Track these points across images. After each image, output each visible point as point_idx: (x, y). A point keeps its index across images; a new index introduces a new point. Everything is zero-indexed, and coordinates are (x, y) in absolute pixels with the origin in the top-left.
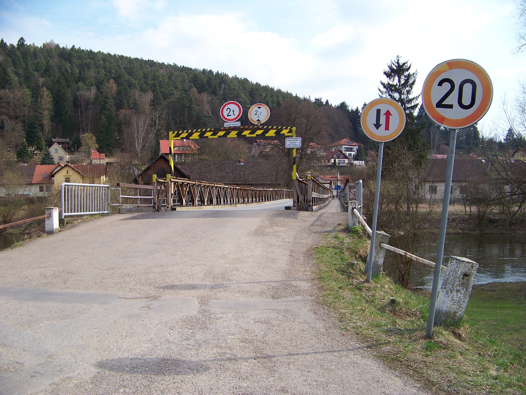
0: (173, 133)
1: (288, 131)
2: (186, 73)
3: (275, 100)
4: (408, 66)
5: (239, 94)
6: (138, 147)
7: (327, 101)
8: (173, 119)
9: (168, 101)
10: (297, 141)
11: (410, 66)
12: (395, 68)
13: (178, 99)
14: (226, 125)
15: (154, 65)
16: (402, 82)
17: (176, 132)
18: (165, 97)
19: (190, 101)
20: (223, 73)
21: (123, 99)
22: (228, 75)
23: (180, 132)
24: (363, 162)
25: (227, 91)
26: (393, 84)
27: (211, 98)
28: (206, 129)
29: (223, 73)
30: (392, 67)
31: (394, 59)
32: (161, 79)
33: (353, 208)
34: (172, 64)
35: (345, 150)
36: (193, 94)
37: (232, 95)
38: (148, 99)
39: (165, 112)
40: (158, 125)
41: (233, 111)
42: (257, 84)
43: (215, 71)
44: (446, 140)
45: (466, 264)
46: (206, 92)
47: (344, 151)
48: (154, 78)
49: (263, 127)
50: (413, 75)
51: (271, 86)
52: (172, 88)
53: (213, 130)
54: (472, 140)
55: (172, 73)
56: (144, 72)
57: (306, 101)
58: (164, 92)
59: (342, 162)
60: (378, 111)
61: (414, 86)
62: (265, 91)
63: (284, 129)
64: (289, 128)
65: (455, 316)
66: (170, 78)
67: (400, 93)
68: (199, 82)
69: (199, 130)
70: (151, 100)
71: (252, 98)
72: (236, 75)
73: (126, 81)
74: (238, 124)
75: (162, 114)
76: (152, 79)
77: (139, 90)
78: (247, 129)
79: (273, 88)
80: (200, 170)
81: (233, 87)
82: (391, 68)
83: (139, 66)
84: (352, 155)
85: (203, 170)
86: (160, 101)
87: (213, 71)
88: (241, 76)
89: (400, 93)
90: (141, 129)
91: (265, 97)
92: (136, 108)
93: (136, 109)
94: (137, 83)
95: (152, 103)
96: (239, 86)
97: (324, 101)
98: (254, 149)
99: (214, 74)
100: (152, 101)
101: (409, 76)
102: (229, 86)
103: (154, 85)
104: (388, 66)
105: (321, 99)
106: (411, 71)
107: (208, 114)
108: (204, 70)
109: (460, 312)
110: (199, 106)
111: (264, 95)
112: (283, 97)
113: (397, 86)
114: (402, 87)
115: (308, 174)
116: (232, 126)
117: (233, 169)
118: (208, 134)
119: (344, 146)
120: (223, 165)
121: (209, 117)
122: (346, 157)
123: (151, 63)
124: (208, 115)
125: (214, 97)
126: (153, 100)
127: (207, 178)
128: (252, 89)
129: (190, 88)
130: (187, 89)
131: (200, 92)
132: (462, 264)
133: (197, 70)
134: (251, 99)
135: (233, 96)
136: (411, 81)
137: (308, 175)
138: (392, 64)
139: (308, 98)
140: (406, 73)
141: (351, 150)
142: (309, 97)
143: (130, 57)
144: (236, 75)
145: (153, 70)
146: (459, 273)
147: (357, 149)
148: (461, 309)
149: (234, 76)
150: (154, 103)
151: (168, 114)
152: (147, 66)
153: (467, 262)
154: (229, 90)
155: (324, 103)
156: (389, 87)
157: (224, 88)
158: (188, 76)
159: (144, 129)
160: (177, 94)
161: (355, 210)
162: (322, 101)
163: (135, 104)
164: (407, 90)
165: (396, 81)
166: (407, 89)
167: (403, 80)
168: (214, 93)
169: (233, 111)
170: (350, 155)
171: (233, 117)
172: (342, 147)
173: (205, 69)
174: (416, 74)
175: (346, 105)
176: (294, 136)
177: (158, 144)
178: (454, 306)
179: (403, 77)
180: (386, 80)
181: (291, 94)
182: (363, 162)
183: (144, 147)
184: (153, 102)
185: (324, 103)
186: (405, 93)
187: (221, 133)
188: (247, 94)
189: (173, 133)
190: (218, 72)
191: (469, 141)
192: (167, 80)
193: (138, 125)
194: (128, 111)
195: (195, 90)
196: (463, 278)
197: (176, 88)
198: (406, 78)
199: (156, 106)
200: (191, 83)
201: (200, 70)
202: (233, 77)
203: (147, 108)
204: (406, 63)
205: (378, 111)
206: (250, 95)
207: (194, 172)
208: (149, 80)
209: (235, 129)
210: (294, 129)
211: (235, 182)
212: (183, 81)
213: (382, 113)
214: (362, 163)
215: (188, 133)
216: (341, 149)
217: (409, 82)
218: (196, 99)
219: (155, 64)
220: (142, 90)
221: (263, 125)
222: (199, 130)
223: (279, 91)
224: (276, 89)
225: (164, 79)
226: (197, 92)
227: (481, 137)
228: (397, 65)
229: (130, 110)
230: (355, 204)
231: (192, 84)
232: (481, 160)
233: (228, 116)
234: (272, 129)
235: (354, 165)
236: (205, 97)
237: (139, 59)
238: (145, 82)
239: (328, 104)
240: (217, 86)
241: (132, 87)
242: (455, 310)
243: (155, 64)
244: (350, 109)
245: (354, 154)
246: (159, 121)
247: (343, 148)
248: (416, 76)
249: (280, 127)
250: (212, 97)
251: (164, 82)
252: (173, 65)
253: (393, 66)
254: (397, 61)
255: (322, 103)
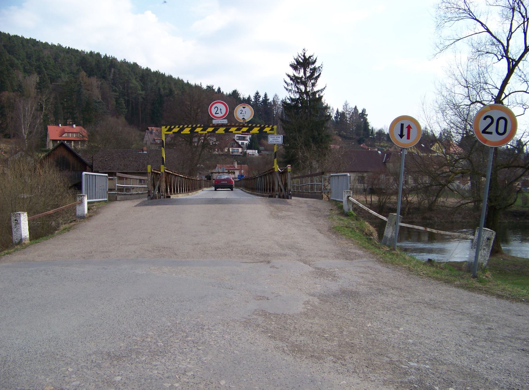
0: (166, 128)
1: (269, 129)
2: (72, 54)
3: (166, 87)
4: (314, 60)
5: (130, 79)
6: (25, 132)
7: (219, 89)
8: (62, 104)
9: (55, 84)
10: (279, 138)
11: (316, 59)
12: (301, 61)
13: (67, 82)
14: (214, 122)
15: (36, 44)
16: (308, 74)
17: (168, 127)
18: (52, 80)
19: (79, 85)
20: (112, 57)
21: (5, 80)
22: (116, 59)
23: (173, 127)
24: (257, 151)
25: (117, 76)
26: (299, 76)
27: (101, 83)
28: (196, 126)
29: (112, 57)
30: (298, 60)
31: (301, 53)
32: (46, 60)
33: (348, 197)
34: (57, 45)
35: (238, 138)
36: (82, 77)
37: (122, 80)
38: (34, 81)
39: (53, 95)
40: (46, 110)
41: (221, 110)
42: (147, 69)
43: (103, 54)
44: (336, 131)
45: (489, 232)
46: (96, 76)
47: (237, 140)
48: (38, 60)
49: (248, 125)
50: (319, 68)
51: (162, 71)
52: (59, 71)
53: (202, 126)
54: (362, 131)
55: (58, 54)
56: (27, 52)
57: (198, 88)
58: (50, 74)
59: (236, 151)
60: (402, 125)
61: (319, 79)
62: (156, 76)
63: (266, 127)
64: (271, 126)
65: (482, 265)
66: (56, 59)
67: (306, 86)
68: (88, 65)
69: (190, 126)
70: (37, 83)
71: (144, 83)
72: (125, 59)
73: (7, 60)
74: (225, 121)
75: (49, 98)
76: (36, 60)
77: (22, 71)
78: (233, 126)
79: (164, 74)
80: (102, 159)
81: (123, 72)
82: (297, 61)
83: (21, 45)
84: (245, 144)
85: (105, 159)
86: (46, 84)
87: (100, 54)
88: (131, 60)
89: (306, 86)
90: (28, 114)
91: (157, 83)
92: (20, 90)
93: (20, 92)
94: (19, 64)
95: (38, 86)
96: (129, 71)
97: (216, 89)
98: (146, 137)
99: (102, 57)
100: (38, 84)
101: (314, 70)
102: (119, 70)
103: (39, 67)
104: (295, 59)
105: (213, 86)
106: (317, 65)
107: (98, 99)
108: (91, 52)
109: (485, 263)
110: (88, 90)
111: (156, 81)
112: (175, 84)
113: (303, 79)
114: (307, 79)
115: (288, 167)
116: (219, 123)
117: (136, 158)
118: (198, 130)
119: (236, 135)
120: (126, 153)
121: (99, 102)
122: (239, 146)
123: (33, 42)
124: (98, 101)
125: (104, 82)
126: (40, 83)
127: (110, 167)
128: (143, 74)
129: (78, 71)
130: (75, 72)
131: (89, 76)
132: (487, 232)
133: (83, 52)
134: (143, 85)
135: (123, 81)
136: (316, 75)
137: (288, 168)
138: (299, 57)
139: (199, 85)
140: (312, 67)
141: (244, 139)
142: (201, 84)
143: (8, 34)
144: (125, 59)
145: (37, 50)
146: (485, 238)
147: (250, 138)
148: (485, 261)
149: (123, 60)
150: (40, 87)
151: (55, 98)
152: (29, 45)
153: (490, 231)
154: (119, 74)
155: (216, 90)
156: (295, 80)
157: (114, 72)
158: (75, 58)
159: (31, 113)
160: (65, 78)
161: (350, 198)
162: (214, 88)
163: (20, 86)
164: (312, 83)
165: (302, 74)
166: (313, 81)
167: (308, 72)
168: (104, 77)
169: (221, 110)
170: (243, 143)
171: (220, 115)
172: (235, 136)
173: (93, 51)
174: (322, 68)
175: (237, 93)
176: (275, 133)
177: (46, 129)
178: (482, 259)
179: (308, 70)
180: (292, 72)
181: (182, 81)
182: (257, 151)
183: (30, 132)
184: (39, 85)
185: (216, 90)
186: (311, 85)
187: (210, 129)
188: (138, 80)
189: (166, 128)
190: (106, 55)
191: (360, 131)
192: (52, 61)
193: (24, 108)
194: (12, 94)
195: (83, 74)
196: (487, 241)
197: (63, 71)
198: (311, 71)
199: (43, 89)
200: (79, 66)
201: (87, 53)
202: (122, 61)
203: (33, 91)
204: (312, 56)
205: (402, 125)
206: (141, 80)
207: (97, 160)
208: (33, 61)
209: (222, 125)
210: (275, 127)
211: (138, 170)
212: (70, 64)
213: (405, 126)
214: (255, 153)
215: (179, 129)
216: (234, 138)
217: (314, 75)
218: (85, 83)
219: (38, 44)
220: (25, 71)
221: (249, 122)
222: (190, 126)
223: (170, 77)
224: (167, 74)
225: (50, 61)
226: (86, 75)
227: (370, 128)
228: (303, 58)
229: (13, 92)
230: (350, 193)
231: (81, 67)
232: (377, 152)
233: (216, 113)
234: (256, 126)
235: (247, 155)
236: (94, 81)
237: (19, 36)
238: (28, 62)
239: (220, 92)
240: (107, 70)
241: (15, 68)
242: (482, 262)
243: (38, 44)
244: (241, 97)
245: (246, 143)
246: (46, 105)
247: (236, 136)
248: (322, 69)
249: (263, 126)
250: (102, 81)
251: (50, 63)
252: (58, 45)
253: (300, 59)
254: (303, 54)
255: (214, 90)
